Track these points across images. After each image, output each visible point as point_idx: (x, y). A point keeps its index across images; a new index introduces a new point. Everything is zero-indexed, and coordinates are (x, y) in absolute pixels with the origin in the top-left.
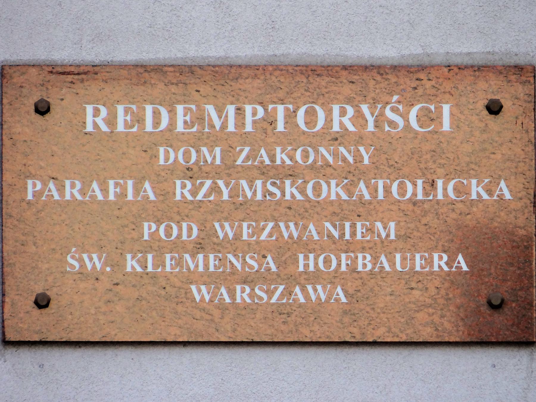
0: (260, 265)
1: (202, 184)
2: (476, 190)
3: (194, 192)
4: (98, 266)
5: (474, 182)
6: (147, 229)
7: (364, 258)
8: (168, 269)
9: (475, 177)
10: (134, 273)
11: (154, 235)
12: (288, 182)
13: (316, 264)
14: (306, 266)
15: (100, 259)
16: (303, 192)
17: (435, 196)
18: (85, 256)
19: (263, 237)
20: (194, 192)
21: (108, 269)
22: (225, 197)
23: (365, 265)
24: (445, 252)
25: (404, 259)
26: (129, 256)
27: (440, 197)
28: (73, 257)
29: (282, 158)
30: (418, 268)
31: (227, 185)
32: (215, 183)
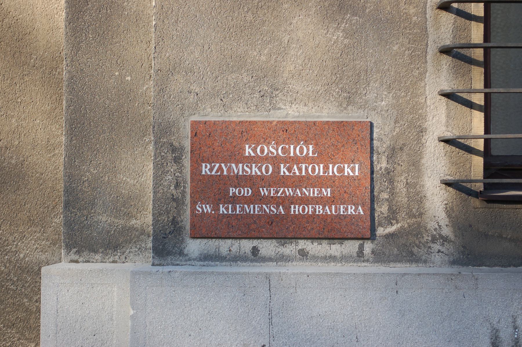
0: (277, 211)
1: (215, 166)
2: (347, 171)
3: (211, 170)
4: (209, 211)
5: (346, 166)
6: (232, 191)
7: (319, 208)
8: (238, 212)
9: (255, 163)
10: (223, 214)
11: (234, 193)
12: (254, 165)
13: (299, 211)
14: (294, 211)
15: (210, 208)
16: (261, 171)
17: (328, 173)
18: (204, 206)
19: (279, 195)
20: (211, 170)
21: (213, 212)
22: (225, 173)
23: (319, 212)
24: (354, 205)
25: (336, 207)
26: (221, 206)
27: (331, 174)
28: (199, 207)
29: (249, 152)
30: (342, 213)
31: (226, 166)
32: (220, 166)
